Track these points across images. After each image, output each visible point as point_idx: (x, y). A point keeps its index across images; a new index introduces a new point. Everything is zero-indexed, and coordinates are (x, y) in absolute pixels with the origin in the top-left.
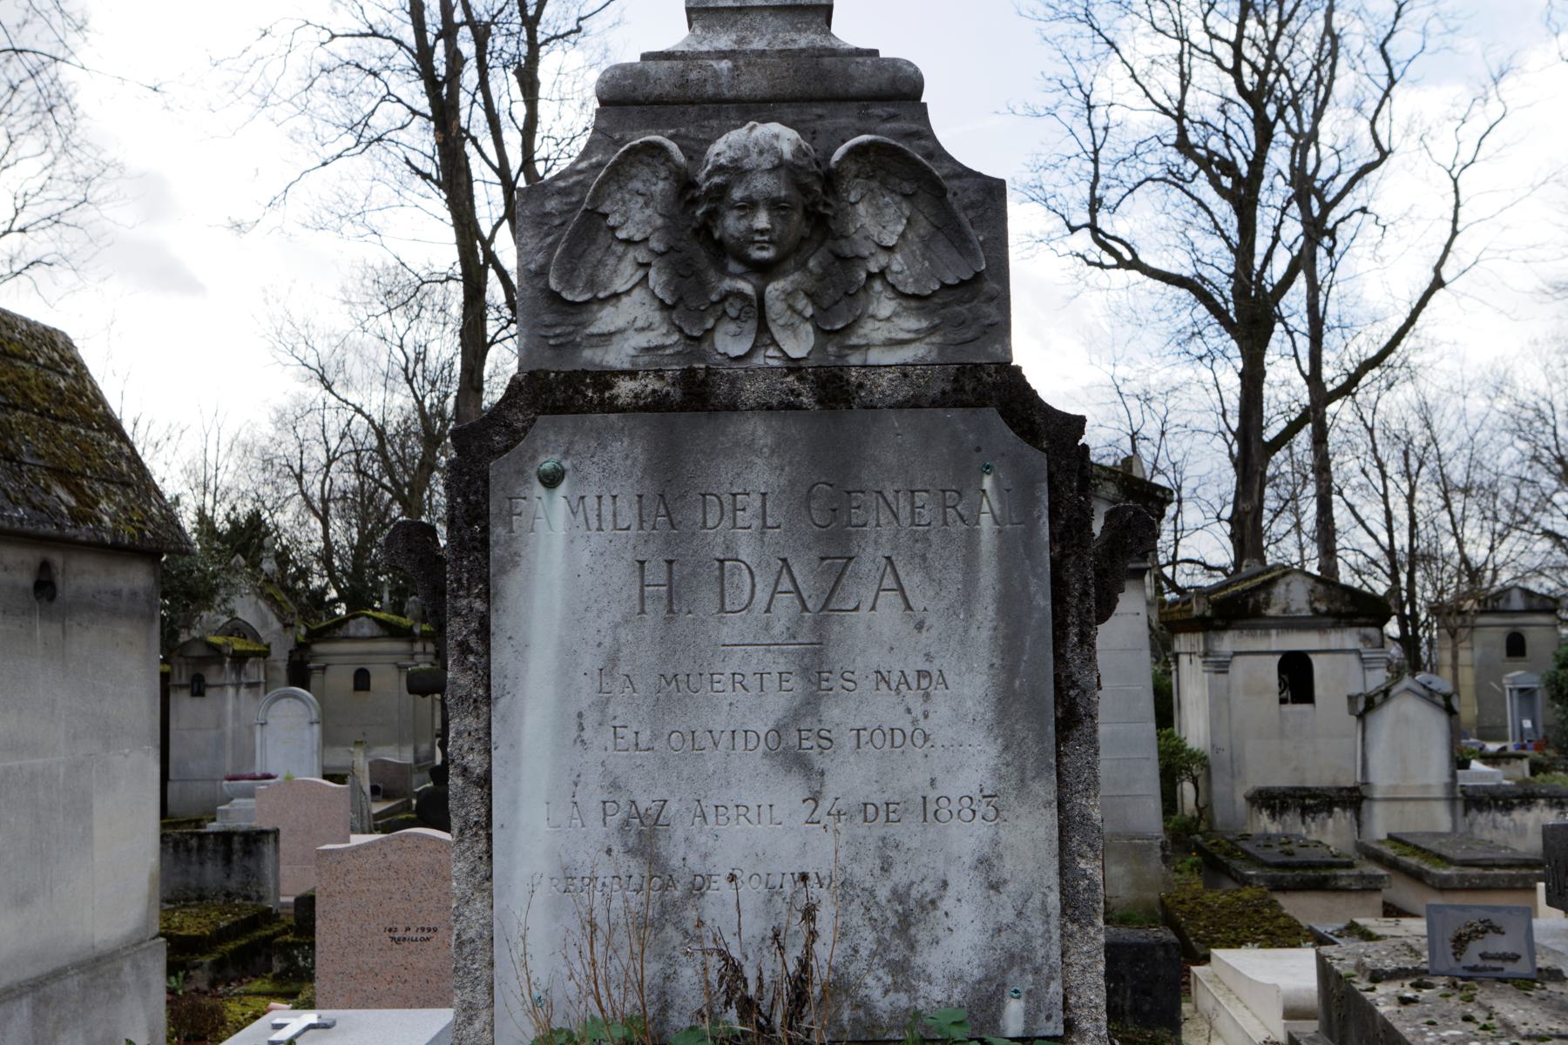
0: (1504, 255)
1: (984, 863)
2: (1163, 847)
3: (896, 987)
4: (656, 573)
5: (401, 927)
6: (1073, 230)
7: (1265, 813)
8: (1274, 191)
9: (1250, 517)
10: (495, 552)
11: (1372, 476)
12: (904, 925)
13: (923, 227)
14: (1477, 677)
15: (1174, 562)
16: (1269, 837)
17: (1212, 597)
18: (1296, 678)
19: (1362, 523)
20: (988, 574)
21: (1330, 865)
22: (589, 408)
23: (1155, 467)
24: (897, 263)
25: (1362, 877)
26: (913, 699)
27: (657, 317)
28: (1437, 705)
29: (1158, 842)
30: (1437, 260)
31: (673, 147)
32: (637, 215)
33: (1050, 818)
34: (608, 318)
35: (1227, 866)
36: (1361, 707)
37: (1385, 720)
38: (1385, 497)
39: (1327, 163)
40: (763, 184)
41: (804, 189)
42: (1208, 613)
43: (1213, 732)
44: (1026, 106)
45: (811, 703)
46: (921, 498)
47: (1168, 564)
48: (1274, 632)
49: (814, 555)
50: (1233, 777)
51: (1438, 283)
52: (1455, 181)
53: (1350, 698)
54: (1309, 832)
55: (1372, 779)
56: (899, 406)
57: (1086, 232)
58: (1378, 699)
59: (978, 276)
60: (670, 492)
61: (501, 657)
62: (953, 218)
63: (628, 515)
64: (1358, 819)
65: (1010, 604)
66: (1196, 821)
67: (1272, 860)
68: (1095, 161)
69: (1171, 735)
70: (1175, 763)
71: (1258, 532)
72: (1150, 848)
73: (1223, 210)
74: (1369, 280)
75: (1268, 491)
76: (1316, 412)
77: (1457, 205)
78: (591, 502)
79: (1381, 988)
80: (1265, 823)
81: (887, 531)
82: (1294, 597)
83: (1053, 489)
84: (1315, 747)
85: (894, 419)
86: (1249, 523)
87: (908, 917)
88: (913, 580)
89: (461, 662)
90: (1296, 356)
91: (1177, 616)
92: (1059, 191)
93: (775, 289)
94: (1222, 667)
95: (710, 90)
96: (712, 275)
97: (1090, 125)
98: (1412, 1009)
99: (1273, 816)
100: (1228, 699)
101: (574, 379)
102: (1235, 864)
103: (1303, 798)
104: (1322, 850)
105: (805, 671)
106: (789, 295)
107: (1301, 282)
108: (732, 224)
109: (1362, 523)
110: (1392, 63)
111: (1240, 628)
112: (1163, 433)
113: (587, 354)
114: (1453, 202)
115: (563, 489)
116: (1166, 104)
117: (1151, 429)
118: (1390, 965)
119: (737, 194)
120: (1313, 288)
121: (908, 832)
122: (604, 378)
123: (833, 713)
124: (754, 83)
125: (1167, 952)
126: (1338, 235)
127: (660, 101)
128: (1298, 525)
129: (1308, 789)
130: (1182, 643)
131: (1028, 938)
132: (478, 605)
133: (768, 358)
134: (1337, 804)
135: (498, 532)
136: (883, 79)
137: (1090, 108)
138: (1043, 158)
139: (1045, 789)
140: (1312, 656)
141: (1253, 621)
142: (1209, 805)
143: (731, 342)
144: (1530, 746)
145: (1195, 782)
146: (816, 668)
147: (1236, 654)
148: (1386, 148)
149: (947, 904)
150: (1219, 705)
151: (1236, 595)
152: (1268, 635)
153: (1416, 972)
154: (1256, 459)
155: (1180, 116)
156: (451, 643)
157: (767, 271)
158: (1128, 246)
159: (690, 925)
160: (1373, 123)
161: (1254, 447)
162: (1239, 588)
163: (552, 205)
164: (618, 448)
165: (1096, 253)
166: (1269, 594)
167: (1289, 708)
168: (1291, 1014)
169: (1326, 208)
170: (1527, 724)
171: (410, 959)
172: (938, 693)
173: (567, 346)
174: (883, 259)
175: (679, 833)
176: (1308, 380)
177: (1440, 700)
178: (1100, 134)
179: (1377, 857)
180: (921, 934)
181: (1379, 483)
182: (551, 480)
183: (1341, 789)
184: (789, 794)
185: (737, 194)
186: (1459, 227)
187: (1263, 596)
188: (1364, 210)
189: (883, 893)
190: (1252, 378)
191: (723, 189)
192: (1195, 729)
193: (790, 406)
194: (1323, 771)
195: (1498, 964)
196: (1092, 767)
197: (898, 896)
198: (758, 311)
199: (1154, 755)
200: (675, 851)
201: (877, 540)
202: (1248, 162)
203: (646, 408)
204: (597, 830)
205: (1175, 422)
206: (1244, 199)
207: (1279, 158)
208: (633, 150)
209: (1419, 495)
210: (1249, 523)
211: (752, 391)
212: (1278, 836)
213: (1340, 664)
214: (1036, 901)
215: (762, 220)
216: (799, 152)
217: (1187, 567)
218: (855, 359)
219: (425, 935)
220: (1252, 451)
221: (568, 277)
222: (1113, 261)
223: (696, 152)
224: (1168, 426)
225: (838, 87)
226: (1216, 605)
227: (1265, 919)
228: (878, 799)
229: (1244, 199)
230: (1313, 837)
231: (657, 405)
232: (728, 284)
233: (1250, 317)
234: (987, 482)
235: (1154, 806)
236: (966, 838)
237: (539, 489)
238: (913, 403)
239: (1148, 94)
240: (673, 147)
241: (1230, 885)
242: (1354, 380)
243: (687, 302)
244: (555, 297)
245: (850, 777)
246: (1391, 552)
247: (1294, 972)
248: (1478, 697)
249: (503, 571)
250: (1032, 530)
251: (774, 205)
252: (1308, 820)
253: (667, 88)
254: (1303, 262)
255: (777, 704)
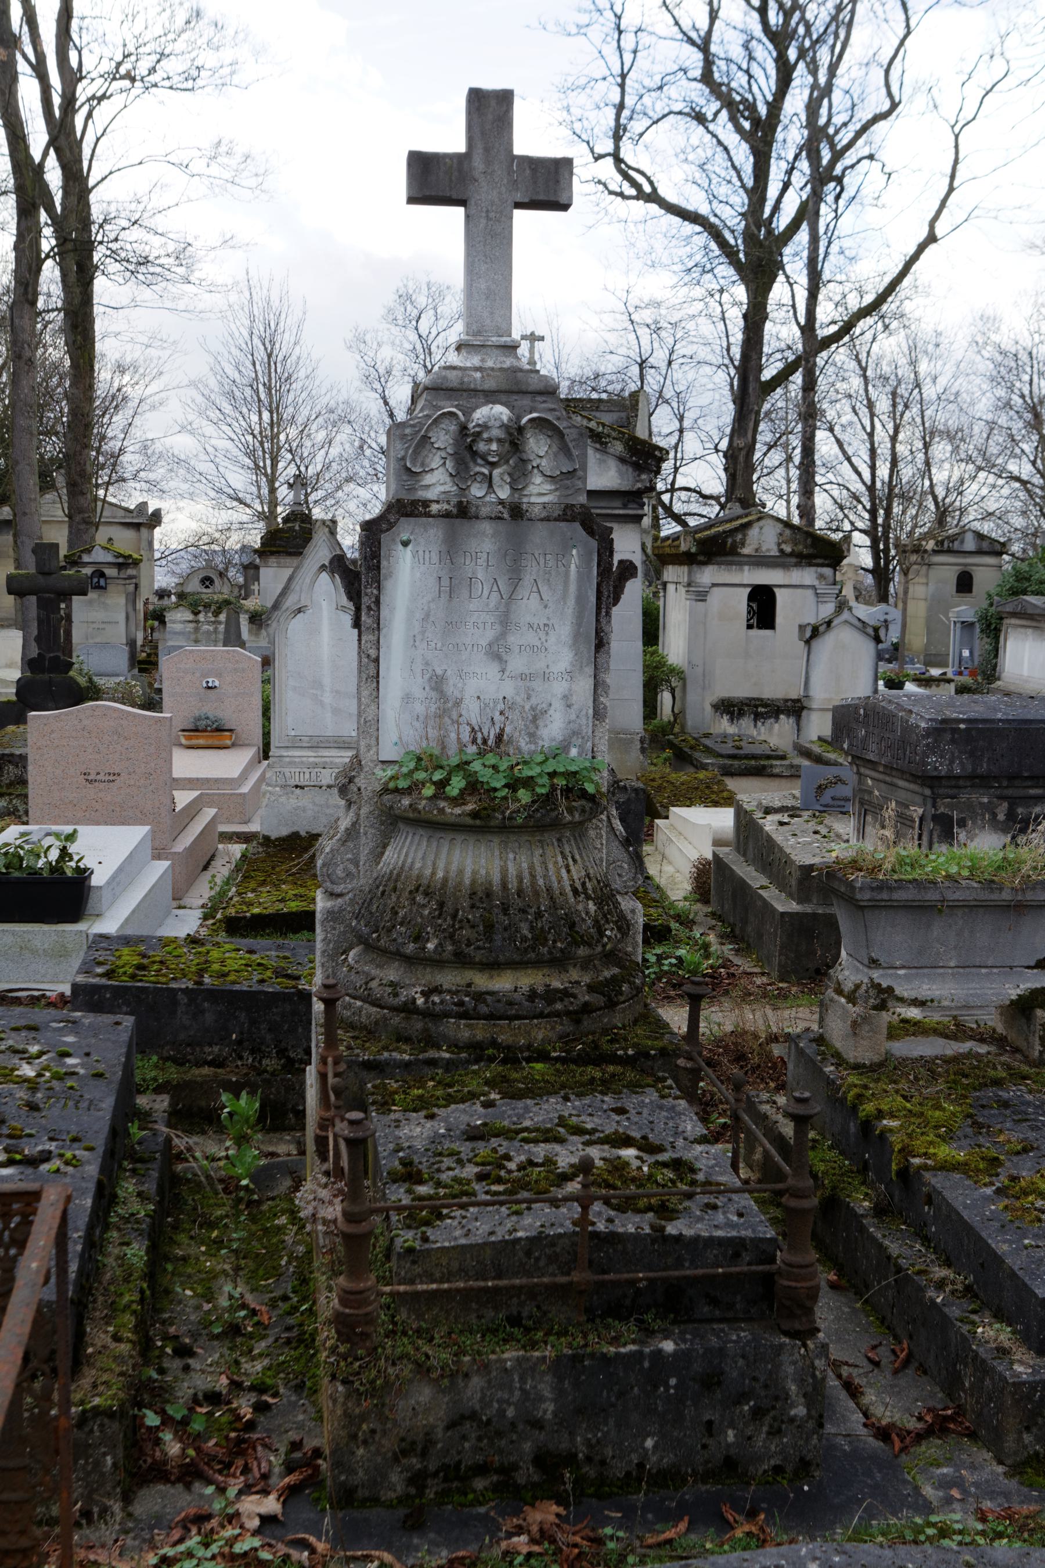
0: (993, 214)
1: (565, 697)
2: (642, 741)
3: (530, 742)
4: (446, 582)
5: (93, 772)
6: (598, 158)
7: (726, 717)
8: (791, 135)
9: (743, 453)
10: (383, 571)
11: (861, 414)
12: (535, 719)
13: (555, 448)
14: (930, 609)
15: (672, 490)
16: (726, 736)
17: (698, 536)
18: (762, 607)
19: (848, 459)
20: (573, 588)
21: (769, 757)
22: (420, 515)
23: (660, 396)
24: (544, 462)
25: (792, 766)
26: (542, 634)
27: (448, 479)
28: (868, 635)
29: (638, 737)
30: (932, 214)
31: (460, 413)
32: (443, 438)
33: (591, 681)
34: (428, 479)
35: (690, 756)
36: (808, 634)
37: (826, 645)
38: (871, 435)
39: (838, 109)
40: (496, 433)
41: (510, 434)
42: (693, 550)
43: (690, 651)
44: (557, 23)
45: (503, 635)
46: (548, 557)
47: (667, 491)
48: (746, 568)
49: (507, 577)
50: (704, 688)
51: (932, 238)
52: (957, 137)
53: (800, 626)
54: (759, 734)
55: (811, 694)
56: (542, 520)
57: (610, 160)
58: (822, 629)
59: (575, 470)
60: (452, 549)
61: (384, 612)
62: (567, 445)
63: (435, 558)
64: (798, 725)
65: (580, 599)
66: (672, 724)
67: (724, 752)
68: (622, 86)
69: (655, 652)
70: (656, 678)
71: (750, 468)
72: (631, 741)
73: (743, 155)
74: (867, 234)
75: (762, 426)
76: (807, 361)
77: (956, 162)
78: (421, 553)
79: (769, 818)
80: (725, 726)
81: (535, 569)
82: (764, 539)
83: (599, 555)
84: (768, 665)
85: (539, 524)
86: (741, 459)
87: (537, 716)
88: (544, 589)
89: (368, 614)
90: (794, 306)
91: (668, 550)
92: (586, 114)
93: (496, 472)
94: (701, 596)
95: (472, 386)
96: (471, 464)
97: (619, 47)
98: (786, 828)
99: (732, 720)
100: (705, 624)
101: (414, 503)
102: (697, 755)
103: (756, 706)
104: (764, 746)
105: (501, 622)
106: (502, 474)
107: (803, 236)
108: (482, 447)
109: (848, 459)
110: (910, 13)
111: (719, 564)
112: (670, 363)
113: (420, 493)
114: (953, 157)
115: (410, 547)
116: (694, 35)
117: (659, 358)
118: (777, 804)
119: (485, 436)
120: (814, 239)
121: (537, 685)
122: (426, 503)
123: (511, 639)
124: (490, 384)
125: (637, 794)
126: (846, 180)
127: (452, 390)
128: (789, 459)
129: (761, 700)
130: (672, 573)
131: (580, 725)
132: (375, 592)
133: (492, 498)
134: (782, 712)
135: (384, 563)
136: (540, 387)
137: (620, 32)
138: (571, 79)
139: (590, 670)
140: (776, 590)
141: (730, 558)
142: (683, 711)
143: (477, 491)
144: (966, 672)
145: (673, 692)
146: (505, 621)
147: (714, 585)
148: (897, 100)
149: (551, 712)
150: (697, 628)
151: (718, 535)
152: (742, 570)
153: (793, 808)
154: (752, 399)
155: (704, 46)
156: (363, 607)
157: (493, 465)
158: (648, 179)
159: (455, 717)
160: (887, 72)
161: (752, 386)
162: (720, 529)
163: (408, 431)
164: (432, 532)
165: (615, 181)
166: (745, 535)
167: (755, 632)
168: (717, 843)
169: (837, 155)
170: (966, 653)
171: (100, 795)
172: (551, 633)
173: (412, 489)
174: (538, 461)
175: (451, 683)
176: (802, 329)
177: (870, 631)
178: (628, 58)
179: (807, 754)
180: (540, 723)
181: (867, 422)
182: (405, 544)
183: (787, 701)
184: (492, 670)
185: (485, 436)
186: (956, 184)
187: (740, 536)
188: (871, 157)
189: (527, 708)
190: (755, 318)
191: (479, 434)
192: (675, 647)
193: (499, 518)
194: (776, 687)
195: (842, 803)
196: (608, 663)
197: (533, 709)
198: (489, 480)
199: (640, 668)
200: (450, 689)
201: (531, 572)
202: (767, 103)
203: (443, 516)
204: (419, 680)
205: (682, 352)
206: (761, 135)
207: (796, 102)
208: (444, 414)
209: (901, 437)
210: (741, 459)
211: (484, 511)
212: (733, 735)
213: (798, 597)
214: (584, 712)
215: (494, 447)
216: (510, 419)
217: (684, 495)
218: (525, 500)
219: (111, 778)
220: (749, 390)
221: (414, 461)
222: (633, 192)
223: (468, 412)
224: (674, 357)
225: (524, 388)
226: (702, 543)
227: (713, 792)
228: (527, 672)
229: (761, 135)
230: (762, 738)
231: (447, 515)
232: (478, 469)
233: (757, 261)
234: (574, 552)
235: (636, 709)
236: (559, 687)
237: (401, 547)
238: (547, 519)
239: (677, 23)
240: (460, 413)
241: (692, 770)
242: (847, 327)
243: (461, 474)
244: (409, 470)
245: (517, 663)
246: (871, 489)
247: (723, 819)
248: (928, 629)
249: (386, 579)
250: (590, 571)
251: (499, 441)
252: (759, 724)
253: (455, 384)
254: (808, 213)
255: (490, 634)
